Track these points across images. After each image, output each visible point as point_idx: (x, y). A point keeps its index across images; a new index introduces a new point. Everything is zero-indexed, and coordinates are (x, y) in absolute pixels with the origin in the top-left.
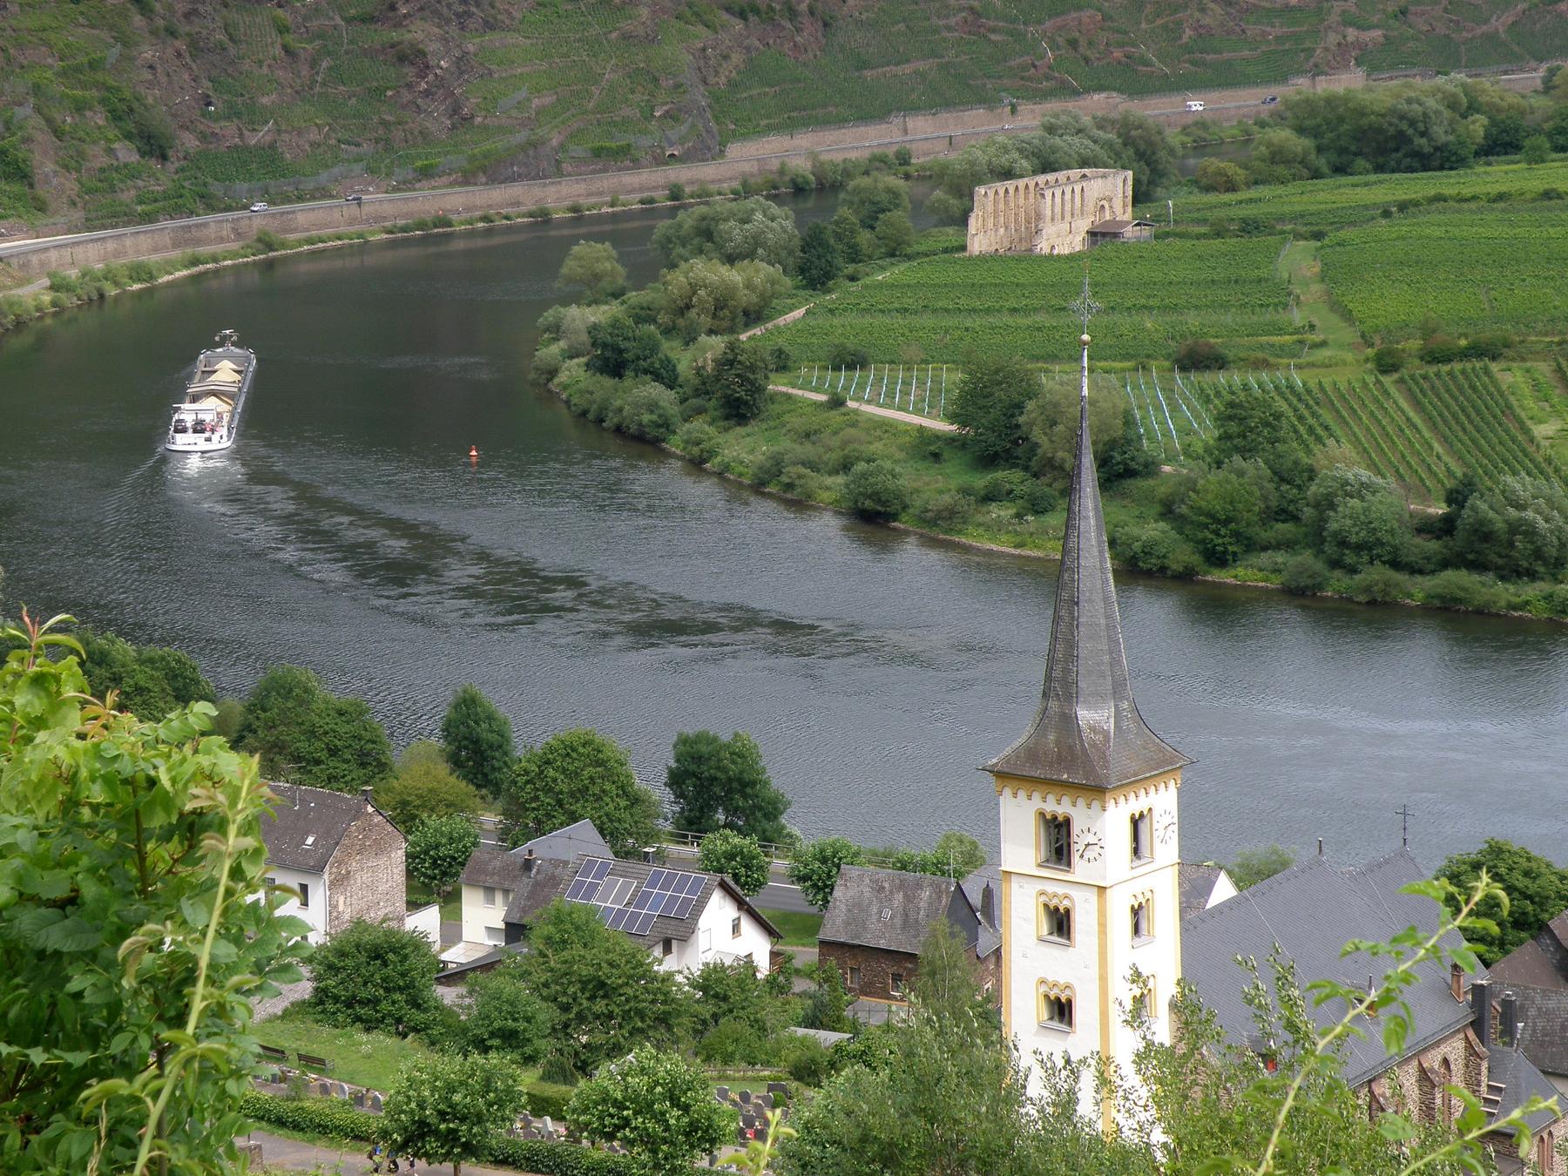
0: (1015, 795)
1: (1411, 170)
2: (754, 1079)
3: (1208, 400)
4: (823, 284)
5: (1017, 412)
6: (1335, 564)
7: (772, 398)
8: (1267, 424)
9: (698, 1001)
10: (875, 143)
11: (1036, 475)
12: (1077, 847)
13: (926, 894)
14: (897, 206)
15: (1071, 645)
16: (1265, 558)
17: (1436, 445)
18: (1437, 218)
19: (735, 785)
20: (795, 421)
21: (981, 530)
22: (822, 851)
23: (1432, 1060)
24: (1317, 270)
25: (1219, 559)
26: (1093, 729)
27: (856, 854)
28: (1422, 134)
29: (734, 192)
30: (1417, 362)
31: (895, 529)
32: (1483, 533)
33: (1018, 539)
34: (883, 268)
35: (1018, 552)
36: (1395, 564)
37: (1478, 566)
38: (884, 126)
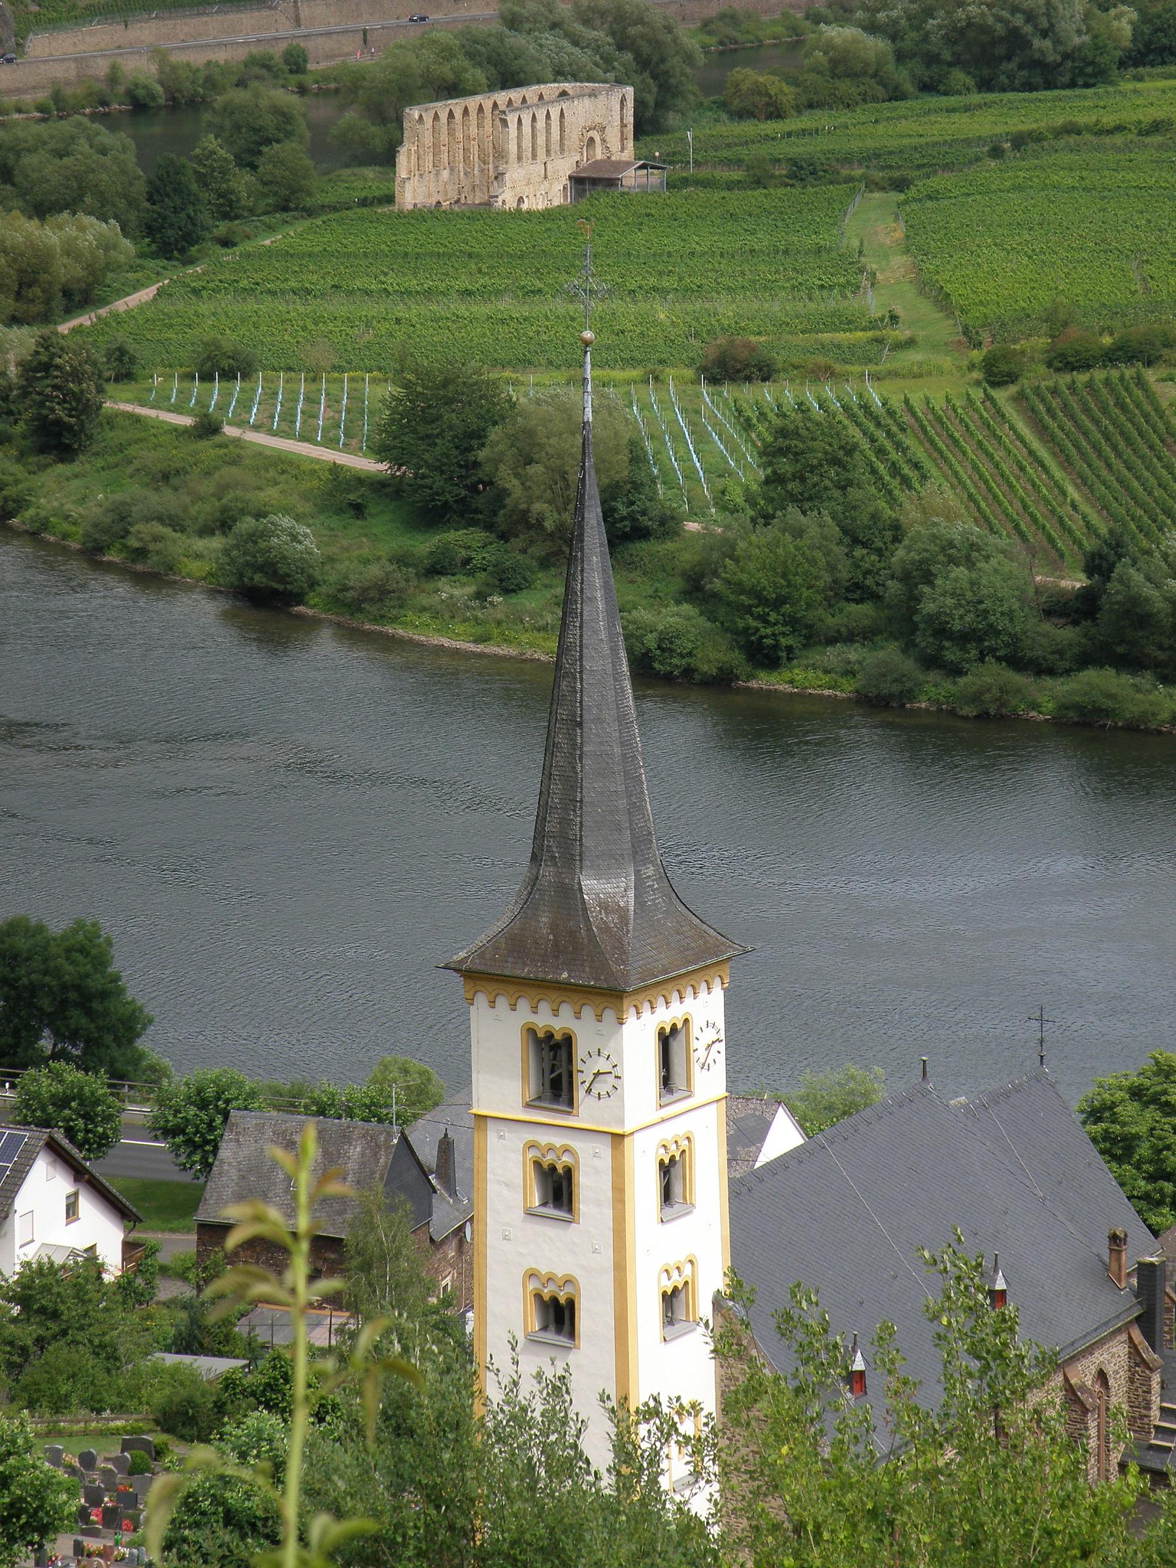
0: (492, 1005)
1: (1029, 87)
2: (101, 1433)
3: (748, 426)
4: (182, 251)
5: (475, 443)
6: (932, 662)
7: (111, 421)
8: (835, 462)
9: (14, 1320)
10: (252, 38)
11: (504, 537)
12: (582, 1079)
13: (356, 1151)
14: (289, 134)
15: (572, 784)
16: (832, 655)
17: (1071, 490)
18: (1068, 158)
19: (72, 995)
20: (147, 456)
21: (426, 617)
22: (199, 1091)
23: (1083, 1374)
24: (899, 234)
25: (767, 657)
26: (605, 906)
27: (252, 1095)
28: (1044, 34)
29: (41, 108)
30: (1042, 369)
31: (300, 617)
32: (1136, 615)
33: (479, 630)
34: (271, 228)
35: (480, 648)
36: (1016, 662)
37: (1130, 663)
38: (265, 13)
